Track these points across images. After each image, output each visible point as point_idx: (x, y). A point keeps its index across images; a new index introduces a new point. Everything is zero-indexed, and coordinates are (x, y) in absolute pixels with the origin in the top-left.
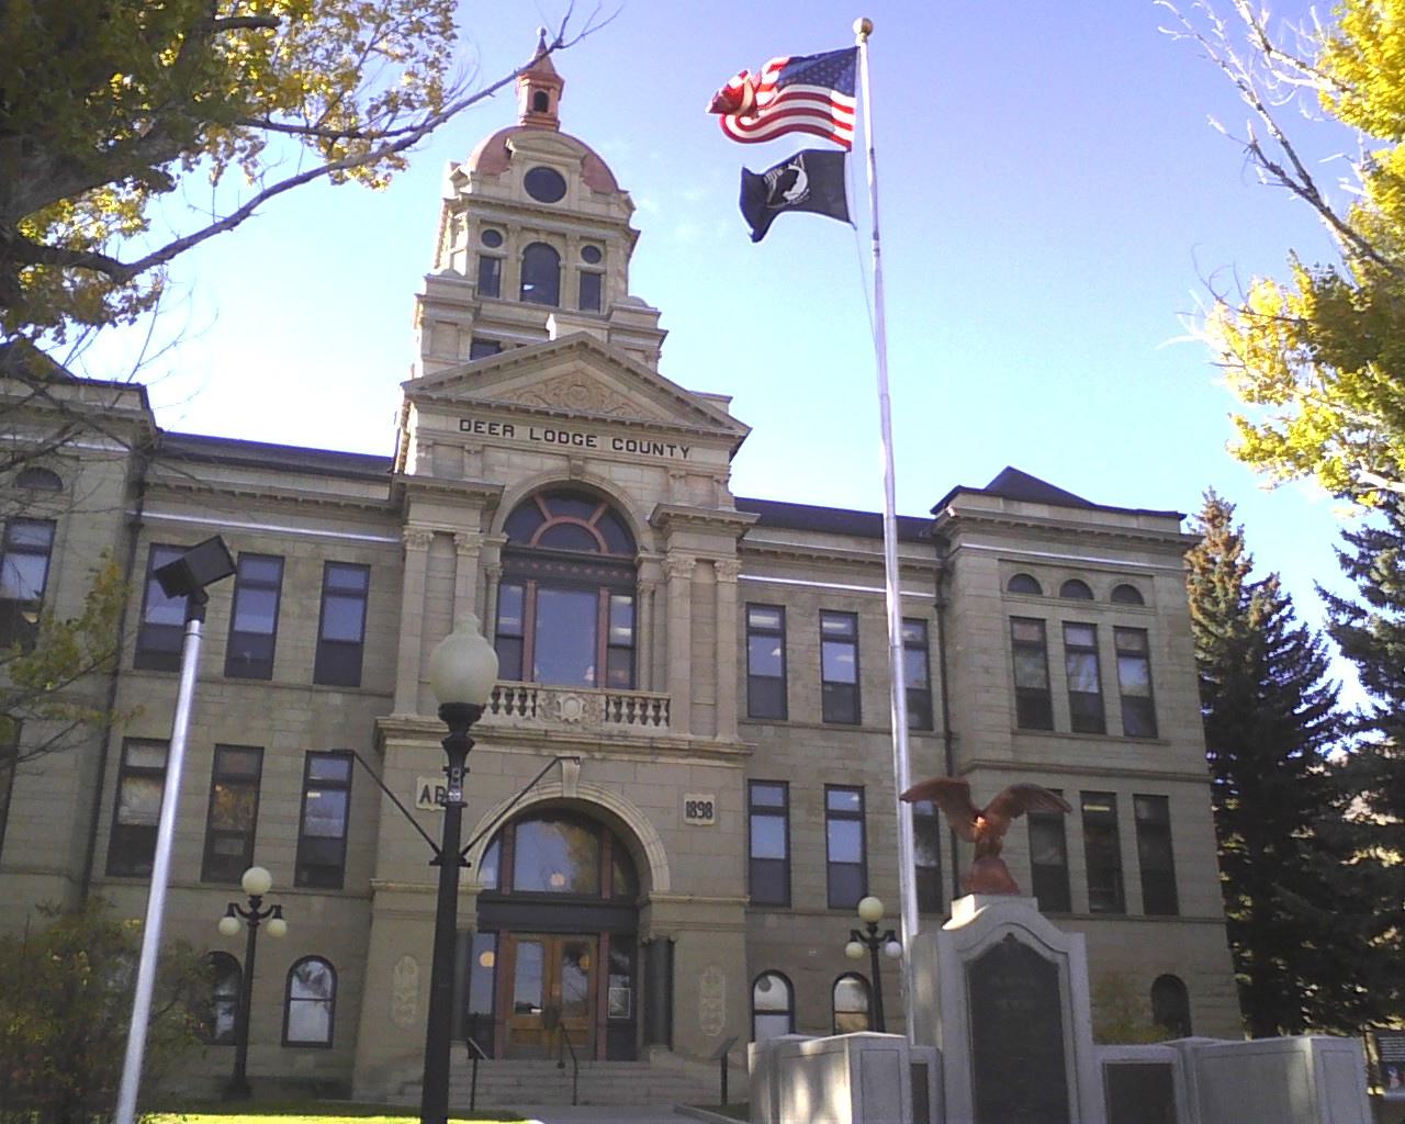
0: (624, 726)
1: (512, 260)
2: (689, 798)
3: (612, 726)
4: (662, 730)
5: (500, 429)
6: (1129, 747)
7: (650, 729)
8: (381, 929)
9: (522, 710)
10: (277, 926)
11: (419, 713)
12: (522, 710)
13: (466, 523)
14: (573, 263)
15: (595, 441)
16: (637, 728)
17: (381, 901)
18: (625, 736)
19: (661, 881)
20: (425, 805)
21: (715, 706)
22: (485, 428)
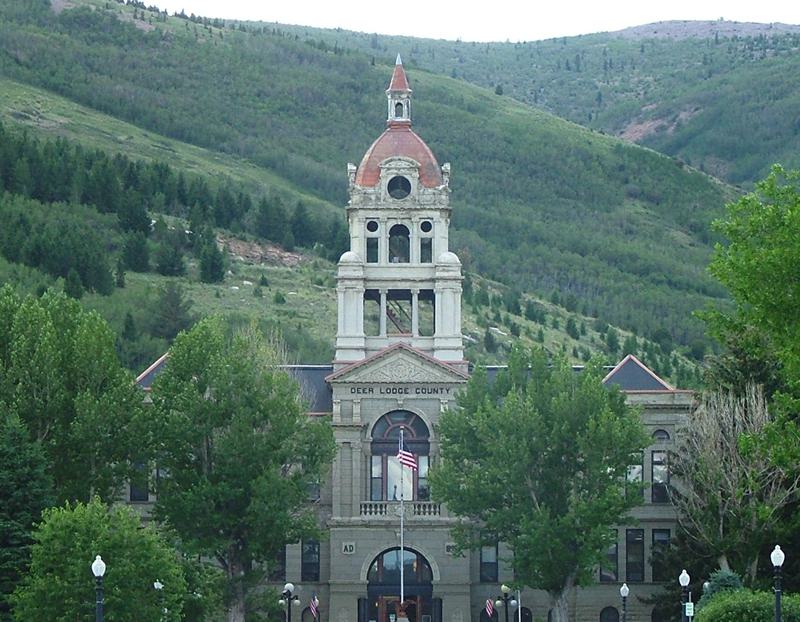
0: (422, 517)
1: (383, 238)
2: (448, 544)
3: (417, 517)
4: (436, 517)
5: (367, 391)
6: (653, 508)
7: (433, 517)
8: (334, 599)
9: (381, 513)
10: (297, 602)
11: (342, 516)
12: (381, 513)
13: (354, 437)
14: (416, 235)
15: (408, 391)
16: (426, 517)
17: (332, 589)
18: (439, 521)
19: (437, 578)
20: (346, 552)
21: (351, 505)
22: (361, 391)
